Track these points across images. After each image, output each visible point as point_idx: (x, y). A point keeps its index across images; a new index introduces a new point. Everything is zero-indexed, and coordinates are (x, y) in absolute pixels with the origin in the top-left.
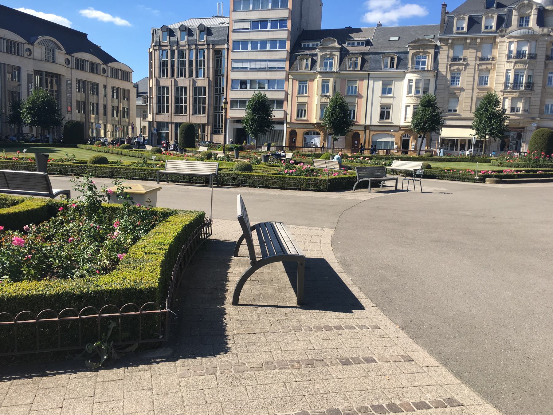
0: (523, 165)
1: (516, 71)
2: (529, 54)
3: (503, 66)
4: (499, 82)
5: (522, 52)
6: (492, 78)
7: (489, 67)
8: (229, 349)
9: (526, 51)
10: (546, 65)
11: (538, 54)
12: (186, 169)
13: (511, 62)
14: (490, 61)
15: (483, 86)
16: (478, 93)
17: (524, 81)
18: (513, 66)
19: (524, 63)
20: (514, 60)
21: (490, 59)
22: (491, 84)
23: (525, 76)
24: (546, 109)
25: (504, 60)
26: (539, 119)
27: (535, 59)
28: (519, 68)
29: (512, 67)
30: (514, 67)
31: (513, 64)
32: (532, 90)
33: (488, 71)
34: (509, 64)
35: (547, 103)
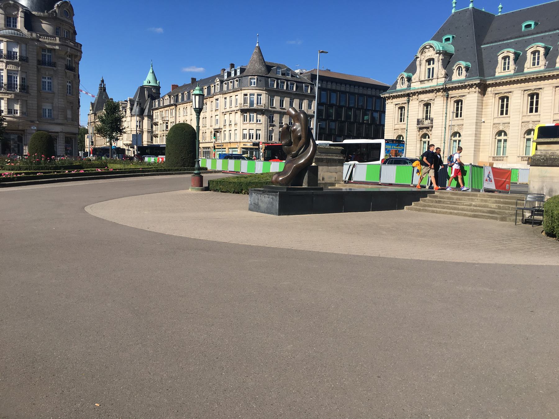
2: (20, 56)
5: (12, 53)
9: (16, 53)
10: (38, 70)
11: (30, 58)
13: (3, 62)
18: (4, 66)
20: (5, 60)
23: (18, 78)
27: (27, 62)
28: (11, 69)
29: (4, 67)
30: (6, 67)
31: (4, 64)
32: (27, 93)
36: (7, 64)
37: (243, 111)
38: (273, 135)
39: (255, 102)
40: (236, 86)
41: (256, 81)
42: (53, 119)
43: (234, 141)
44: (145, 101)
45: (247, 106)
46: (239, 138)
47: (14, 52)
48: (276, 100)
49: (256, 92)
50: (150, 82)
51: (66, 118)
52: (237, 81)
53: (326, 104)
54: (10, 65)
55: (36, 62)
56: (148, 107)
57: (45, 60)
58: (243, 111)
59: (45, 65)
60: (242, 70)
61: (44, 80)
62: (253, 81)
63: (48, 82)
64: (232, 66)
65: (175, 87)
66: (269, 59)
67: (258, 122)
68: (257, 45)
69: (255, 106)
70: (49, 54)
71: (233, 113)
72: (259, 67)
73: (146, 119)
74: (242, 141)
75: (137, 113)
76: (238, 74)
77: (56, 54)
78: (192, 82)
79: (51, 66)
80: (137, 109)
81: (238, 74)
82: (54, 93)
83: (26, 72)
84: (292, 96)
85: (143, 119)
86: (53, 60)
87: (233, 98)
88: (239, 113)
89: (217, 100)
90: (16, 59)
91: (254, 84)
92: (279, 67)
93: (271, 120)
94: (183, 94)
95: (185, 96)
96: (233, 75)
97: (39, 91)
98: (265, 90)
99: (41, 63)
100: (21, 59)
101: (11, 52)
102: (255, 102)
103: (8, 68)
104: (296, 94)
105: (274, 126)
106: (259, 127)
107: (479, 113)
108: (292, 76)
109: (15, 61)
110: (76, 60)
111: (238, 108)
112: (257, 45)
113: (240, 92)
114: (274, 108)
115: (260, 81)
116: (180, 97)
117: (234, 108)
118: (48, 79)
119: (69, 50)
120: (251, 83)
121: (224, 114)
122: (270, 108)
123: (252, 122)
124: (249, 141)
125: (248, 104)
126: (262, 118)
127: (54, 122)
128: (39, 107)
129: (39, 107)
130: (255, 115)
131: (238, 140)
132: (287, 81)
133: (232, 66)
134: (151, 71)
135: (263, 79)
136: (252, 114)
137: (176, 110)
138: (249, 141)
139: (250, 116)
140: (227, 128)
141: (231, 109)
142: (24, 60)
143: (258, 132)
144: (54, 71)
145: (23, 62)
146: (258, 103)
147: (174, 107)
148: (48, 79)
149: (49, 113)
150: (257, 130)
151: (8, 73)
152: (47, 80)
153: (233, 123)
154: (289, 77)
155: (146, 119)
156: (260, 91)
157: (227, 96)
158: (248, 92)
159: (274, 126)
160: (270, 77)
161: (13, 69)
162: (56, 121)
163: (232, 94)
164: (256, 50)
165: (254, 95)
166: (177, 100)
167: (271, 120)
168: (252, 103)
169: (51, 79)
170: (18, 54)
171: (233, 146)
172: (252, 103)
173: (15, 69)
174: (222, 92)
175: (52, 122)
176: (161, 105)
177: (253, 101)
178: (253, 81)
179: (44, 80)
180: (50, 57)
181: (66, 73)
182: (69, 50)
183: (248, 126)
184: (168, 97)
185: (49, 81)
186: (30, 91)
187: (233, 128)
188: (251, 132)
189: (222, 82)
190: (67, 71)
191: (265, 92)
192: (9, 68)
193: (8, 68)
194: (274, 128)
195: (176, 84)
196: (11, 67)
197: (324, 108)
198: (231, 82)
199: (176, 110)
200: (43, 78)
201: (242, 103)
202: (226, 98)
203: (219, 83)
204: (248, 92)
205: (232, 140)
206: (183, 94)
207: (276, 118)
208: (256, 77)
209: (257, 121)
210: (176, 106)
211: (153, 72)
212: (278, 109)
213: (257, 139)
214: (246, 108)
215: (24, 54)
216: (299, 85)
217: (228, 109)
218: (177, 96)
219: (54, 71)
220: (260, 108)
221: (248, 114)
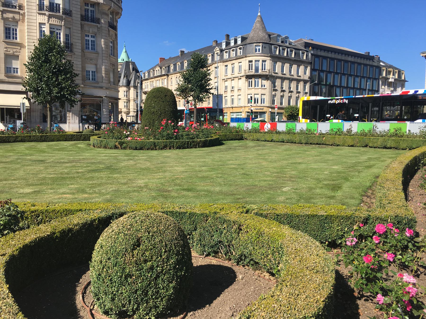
0: (163, 145)
1: (52, 27)
2: (64, 9)
3: (35, 18)
4: (32, 38)
5: (55, 5)
6: (22, 31)
7: (17, 17)
8: (300, 130)
9: (59, 5)
10: (82, 26)
11: (73, 12)
12: (202, 150)
13: (45, 14)
14: (17, 10)
15: (11, 40)
16: (6, 48)
17: (62, 40)
18: (47, 19)
19: (60, 18)
20: (47, 13)
21: (15, 7)
22: (22, 38)
23: (62, 34)
24: (87, 75)
25: (35, 11)
26: (82, 86)
27: (71, 16)
28: (54, 23)
29: (46, 21)
30: (48, 21)
31: (46, 18)
32: (71, 51)
33: (16, 22)
34: (42, 17)
35: (87, 69)
36: (50, 17)
37: (248, 77)
38: (276, 99)
39: (260, 68)
40: (238, 54)
41: (261, 48)
42: (98, 83)
43: (237, 106)
44: (130, 74)
45: (253, 72)
46: (243, 102)
47: (57, 4)
48: (279, 65)
49: (261, 58)
50: (123, 60)
51: (110, 82)
52: (240, 49)
53: (318, 70)
54: (53, 19)
55: (79, 16)
56: (133, 78)
57: (88, 16)
58: (248, 77)
59: (88, 21)
60: (244, 39)
61: (87, 38)
62: (258, 48)
63: (92, 41)
64: (228, 36)
65: (162, 59)
66: (269, 31)
67: (263, 87)
68: (259, 14)
69: (260, 72)
70: (92, 9)
71: (236, 80)
72: (262, 35)
73: (132, 89)
74: (246, 105)
75: (125, 84)
76: (239, 42)
77: (100, 8)
78: (181, 55)
79: (94, 22)
80: (125, 81)
81: (239, 42)
82: (97, 53)
83: (70, 28)
84: (291, 62)
85: (129, 89)
86: (97, 15)
87: (236, 65)
88: (244, 79)
89: (216, 68)
90: (59, 12)
91: (259, 51)
92: (279, 36)
93: (274, 83)
94: (175, 65)
95: (178, 66)
96: (232, 44)
97: (83, 51)
98: (270, 57)
99: (84, 18)
100: (65, 13)
101: (53, 4)
102: (260, 68)
103: (50, 22)
104: (295, 60)
105: (276, 90)
106: (263, 92)
107: (127, 96)
108: (289, 44)
109: (58, 14)
110: (117, 17)
111: (243, 74)
112: (259, 14)
113: (245, 59)
114: (277, 73)
115: (265, 47)
116: (172, 68)
117: (236, 75)
118: (92, 37)
119: (113, 6)
120: (256, 50)
121: (225, 80)
122: (273, 74)
123: (257, 87)
124: (255, 105)
125: (254, 71)
126: (267, 83)
127: (98, 85)
128: (83, 68)
129: (83, 68)
130: (260, 80)
131: (242, 105)
132: (288, 47)
133: (228, 36)
134: (124, 50)
135: (267, 46)
136: (257, 80)
137: (168, 80)
138: (255, 105)
139: (255, 82)
140: (229, 94)
141: (234, 76)
142: (68, 14)
143: (263, 97)
144: (98, 28)
145: (67, 16)
146: (262, 69)
147: (166, 77)
148: (92, 37)
149: (92, 75)
150: (262, 94)
151: (50, 28)
152: (90, 39)
153: (236, 89)
154: (287, 44)
155: (132, 89)
156: (264, 58)
157: (229, 64)
158: (253, 59)
159: (276, 90)
160: (273, 46)
161: (56, 23)
162: (100, 85)
163: (234, 62)
164: (258, 19)
165: (259, 61)
166: (169, 71)
167: (274, 83)
168: (257, 70)
169: (94, 38)
170: (61, 6)
171: (235, 110)
172: (257, 70)
173: (58, 24)
174: (222, 60)
175: (96, 85)
176: (151, 76)
177: (258, 67)
178: (258, 48)
179: (87, 38)
180: (92, 12)
181: (109, 31)
182: (113, 6)
183: (253, 91)
184: (159, 68)
185: (93, 39)
186: (75, 50)
187: (236, 93)
188: (256, 96)
189: (222, 51)
190: (110, 29)
191: (269, 58)
192: (52, 23)
193: (50, 22)
194: (276, 92)
195: (163, 57)
196: (54, 21)
197: (317, 73)
198: (233, 50)
199: (168, 80)
200: (86, 36)
201: (247, 68)
202: (226, 66)
203: (219, 52)
204: (253, 59)
205: (235, 105)
206: (175, 65)
207: (278, 82)
208: (261, 44)
209: (262, 86)
210: (168, 76)
211: (126, 52)
212: (280, 75)
213: (261, 103)
214: (252, 74)
215: (67, 8)
216: (297, 51)
217: (229, 76)
218: (169, 67)
219: (98, 28)
220: (264, 73)
221: (253, 80)
